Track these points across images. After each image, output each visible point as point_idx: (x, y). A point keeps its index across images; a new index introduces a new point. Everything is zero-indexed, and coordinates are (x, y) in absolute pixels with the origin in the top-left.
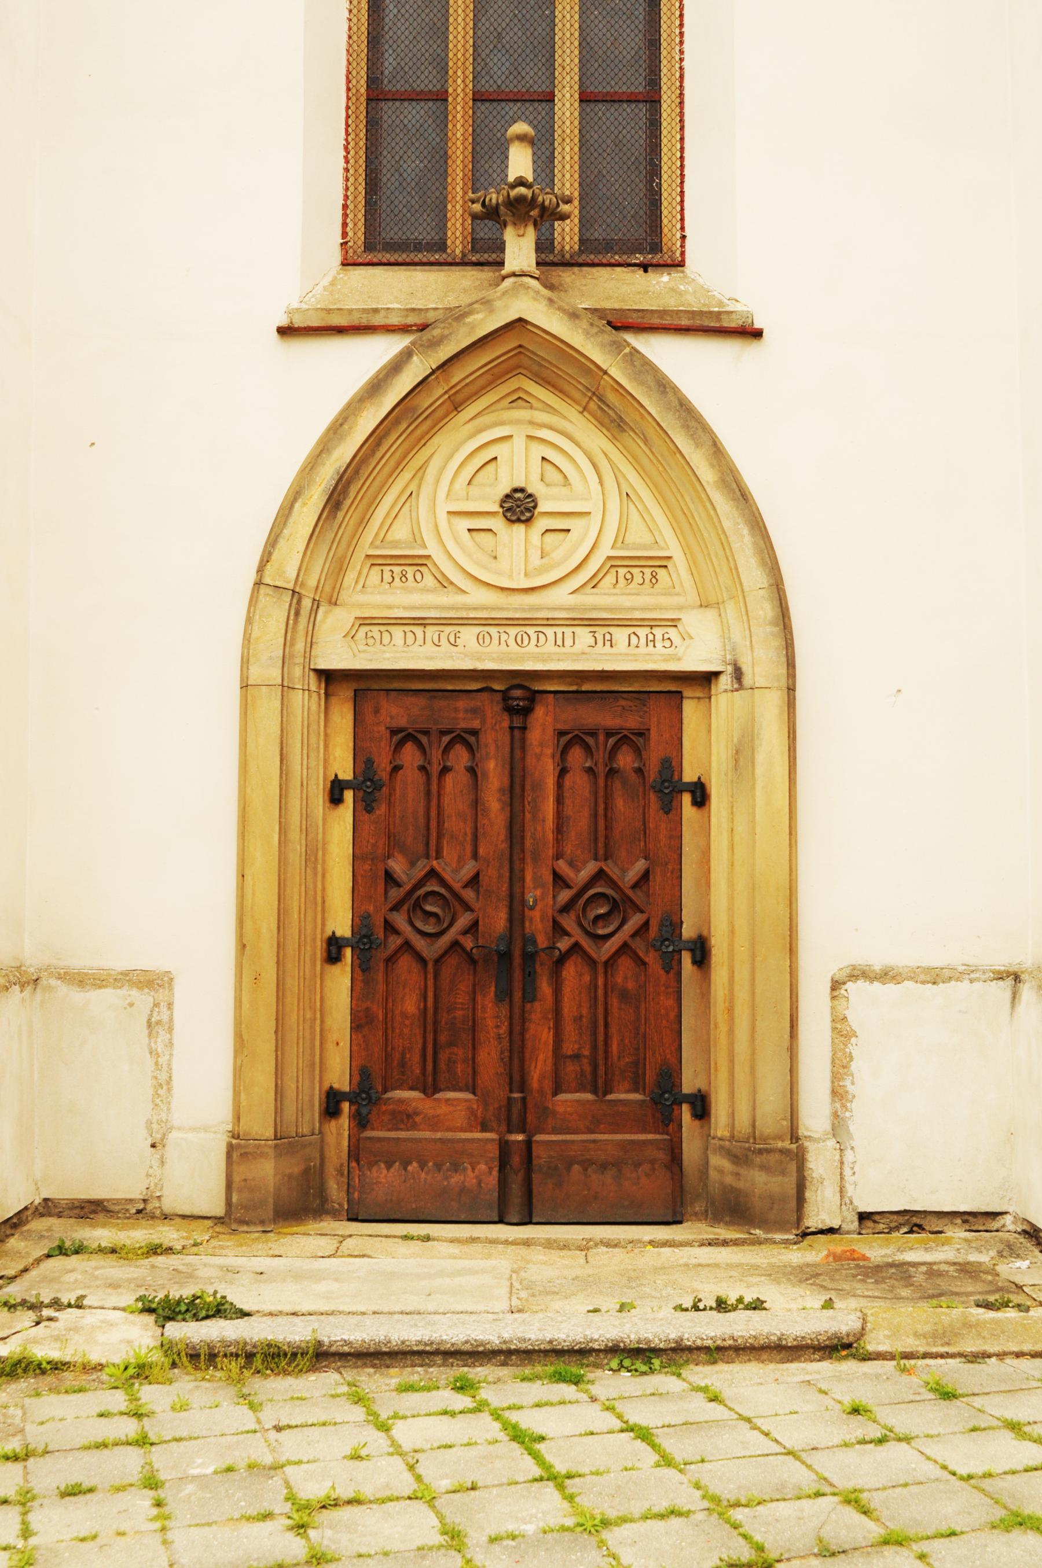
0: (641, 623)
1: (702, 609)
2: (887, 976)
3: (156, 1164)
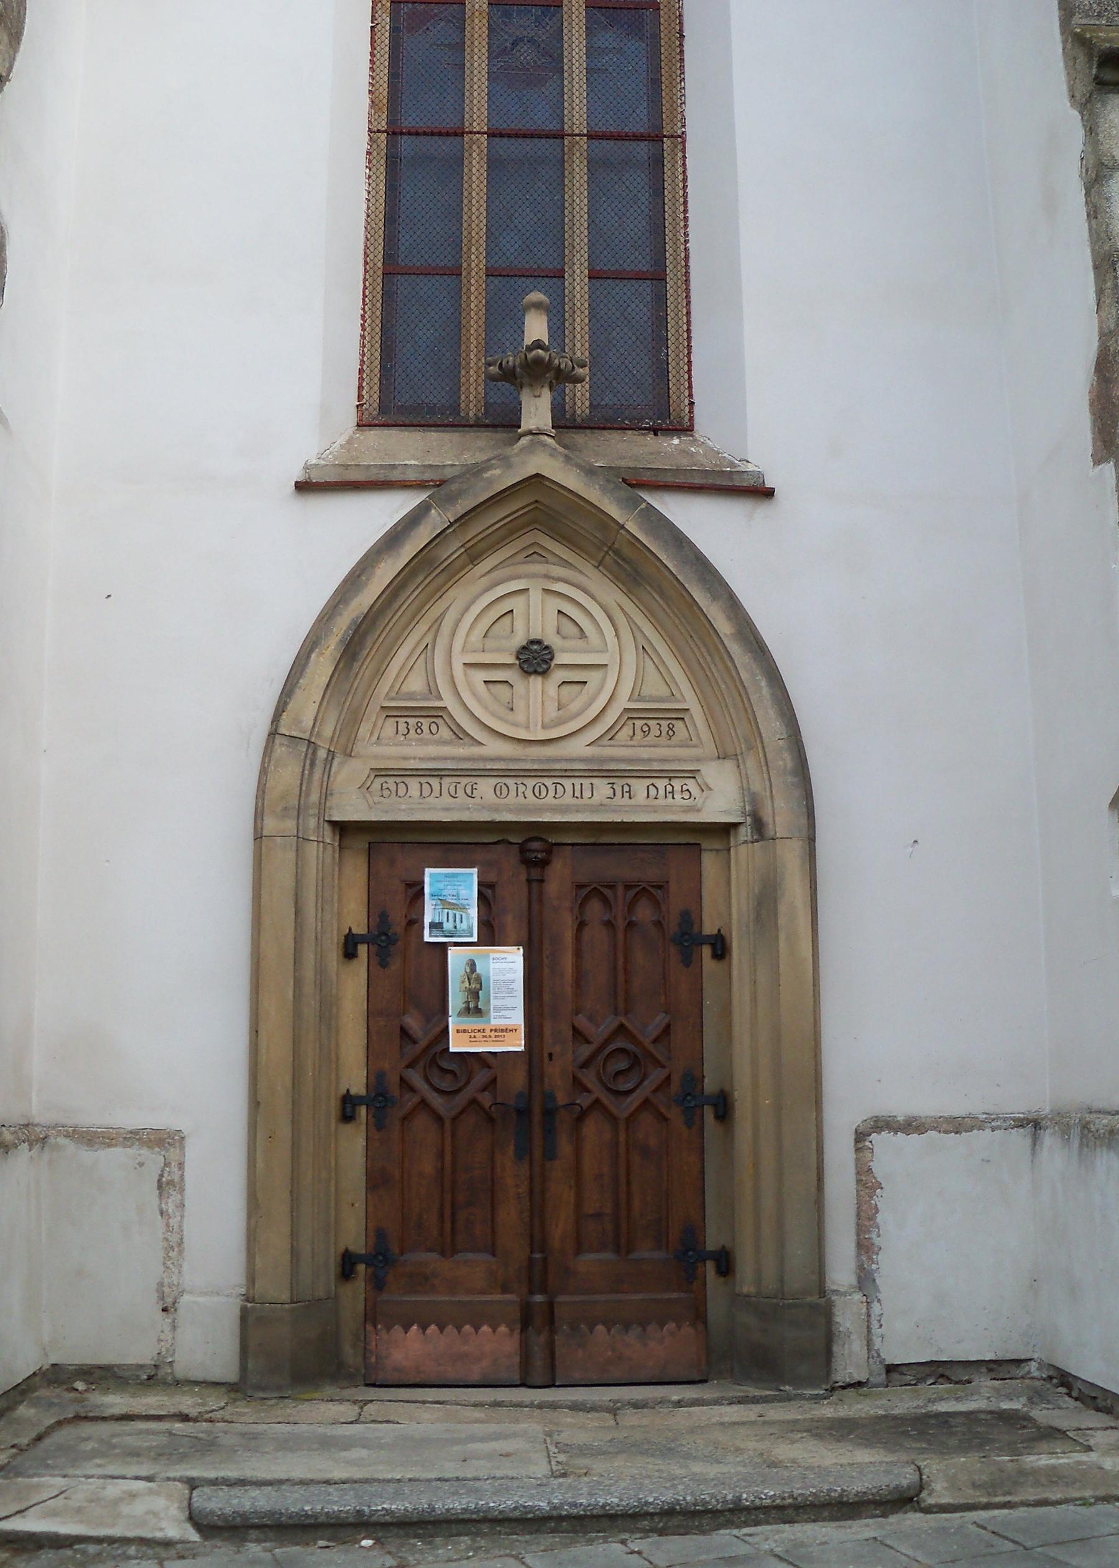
0: (660, 774)
1: (721, 760)
2: (912, 1126)
3: (167, 1329)
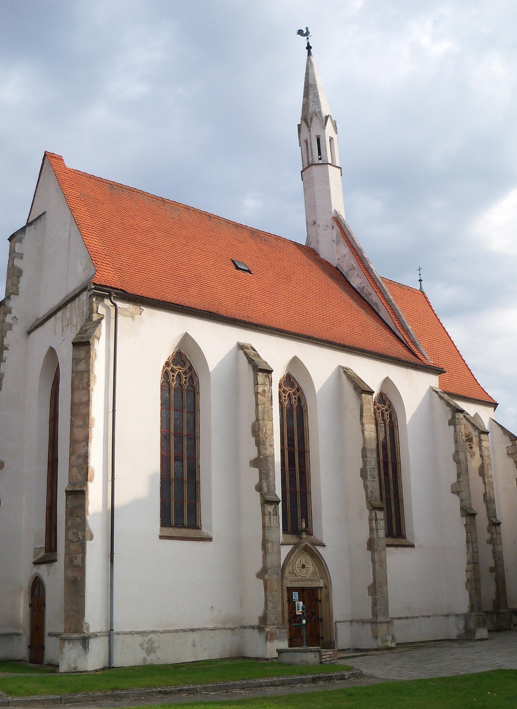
0: (315, 581)
2: (340, 622)
